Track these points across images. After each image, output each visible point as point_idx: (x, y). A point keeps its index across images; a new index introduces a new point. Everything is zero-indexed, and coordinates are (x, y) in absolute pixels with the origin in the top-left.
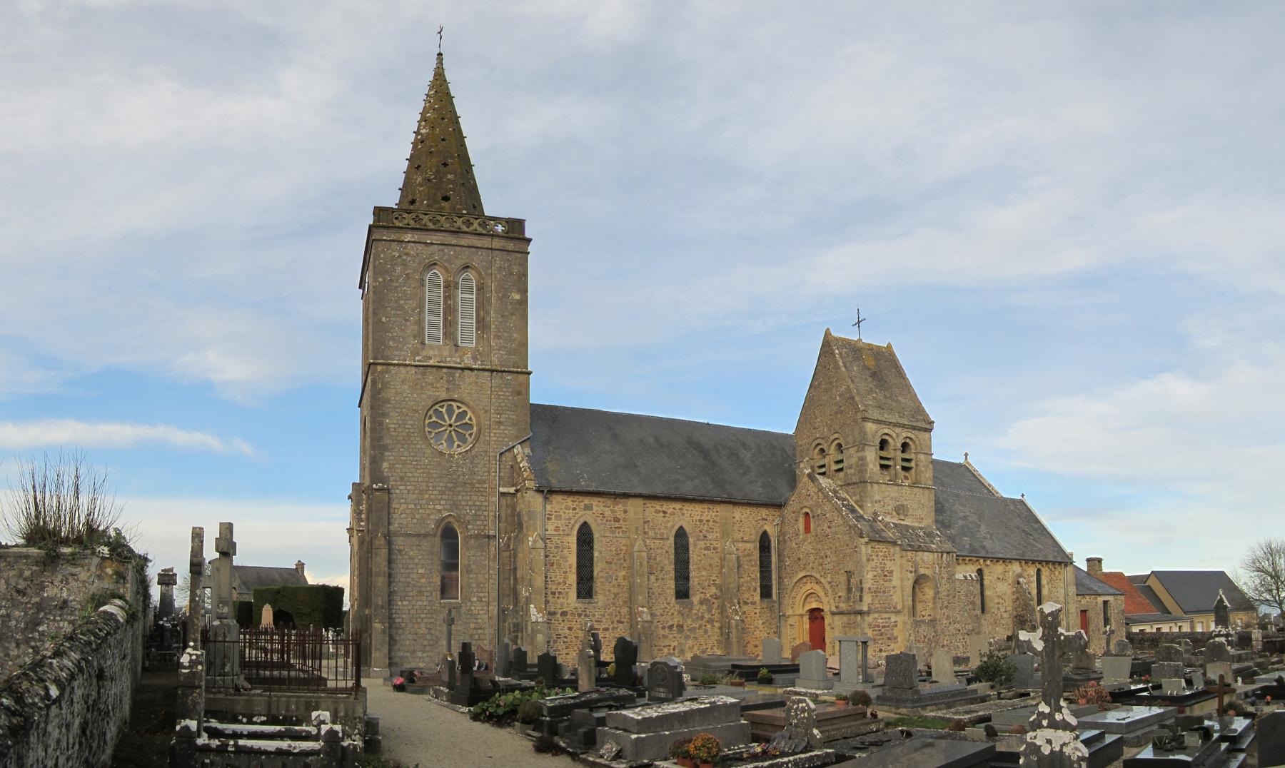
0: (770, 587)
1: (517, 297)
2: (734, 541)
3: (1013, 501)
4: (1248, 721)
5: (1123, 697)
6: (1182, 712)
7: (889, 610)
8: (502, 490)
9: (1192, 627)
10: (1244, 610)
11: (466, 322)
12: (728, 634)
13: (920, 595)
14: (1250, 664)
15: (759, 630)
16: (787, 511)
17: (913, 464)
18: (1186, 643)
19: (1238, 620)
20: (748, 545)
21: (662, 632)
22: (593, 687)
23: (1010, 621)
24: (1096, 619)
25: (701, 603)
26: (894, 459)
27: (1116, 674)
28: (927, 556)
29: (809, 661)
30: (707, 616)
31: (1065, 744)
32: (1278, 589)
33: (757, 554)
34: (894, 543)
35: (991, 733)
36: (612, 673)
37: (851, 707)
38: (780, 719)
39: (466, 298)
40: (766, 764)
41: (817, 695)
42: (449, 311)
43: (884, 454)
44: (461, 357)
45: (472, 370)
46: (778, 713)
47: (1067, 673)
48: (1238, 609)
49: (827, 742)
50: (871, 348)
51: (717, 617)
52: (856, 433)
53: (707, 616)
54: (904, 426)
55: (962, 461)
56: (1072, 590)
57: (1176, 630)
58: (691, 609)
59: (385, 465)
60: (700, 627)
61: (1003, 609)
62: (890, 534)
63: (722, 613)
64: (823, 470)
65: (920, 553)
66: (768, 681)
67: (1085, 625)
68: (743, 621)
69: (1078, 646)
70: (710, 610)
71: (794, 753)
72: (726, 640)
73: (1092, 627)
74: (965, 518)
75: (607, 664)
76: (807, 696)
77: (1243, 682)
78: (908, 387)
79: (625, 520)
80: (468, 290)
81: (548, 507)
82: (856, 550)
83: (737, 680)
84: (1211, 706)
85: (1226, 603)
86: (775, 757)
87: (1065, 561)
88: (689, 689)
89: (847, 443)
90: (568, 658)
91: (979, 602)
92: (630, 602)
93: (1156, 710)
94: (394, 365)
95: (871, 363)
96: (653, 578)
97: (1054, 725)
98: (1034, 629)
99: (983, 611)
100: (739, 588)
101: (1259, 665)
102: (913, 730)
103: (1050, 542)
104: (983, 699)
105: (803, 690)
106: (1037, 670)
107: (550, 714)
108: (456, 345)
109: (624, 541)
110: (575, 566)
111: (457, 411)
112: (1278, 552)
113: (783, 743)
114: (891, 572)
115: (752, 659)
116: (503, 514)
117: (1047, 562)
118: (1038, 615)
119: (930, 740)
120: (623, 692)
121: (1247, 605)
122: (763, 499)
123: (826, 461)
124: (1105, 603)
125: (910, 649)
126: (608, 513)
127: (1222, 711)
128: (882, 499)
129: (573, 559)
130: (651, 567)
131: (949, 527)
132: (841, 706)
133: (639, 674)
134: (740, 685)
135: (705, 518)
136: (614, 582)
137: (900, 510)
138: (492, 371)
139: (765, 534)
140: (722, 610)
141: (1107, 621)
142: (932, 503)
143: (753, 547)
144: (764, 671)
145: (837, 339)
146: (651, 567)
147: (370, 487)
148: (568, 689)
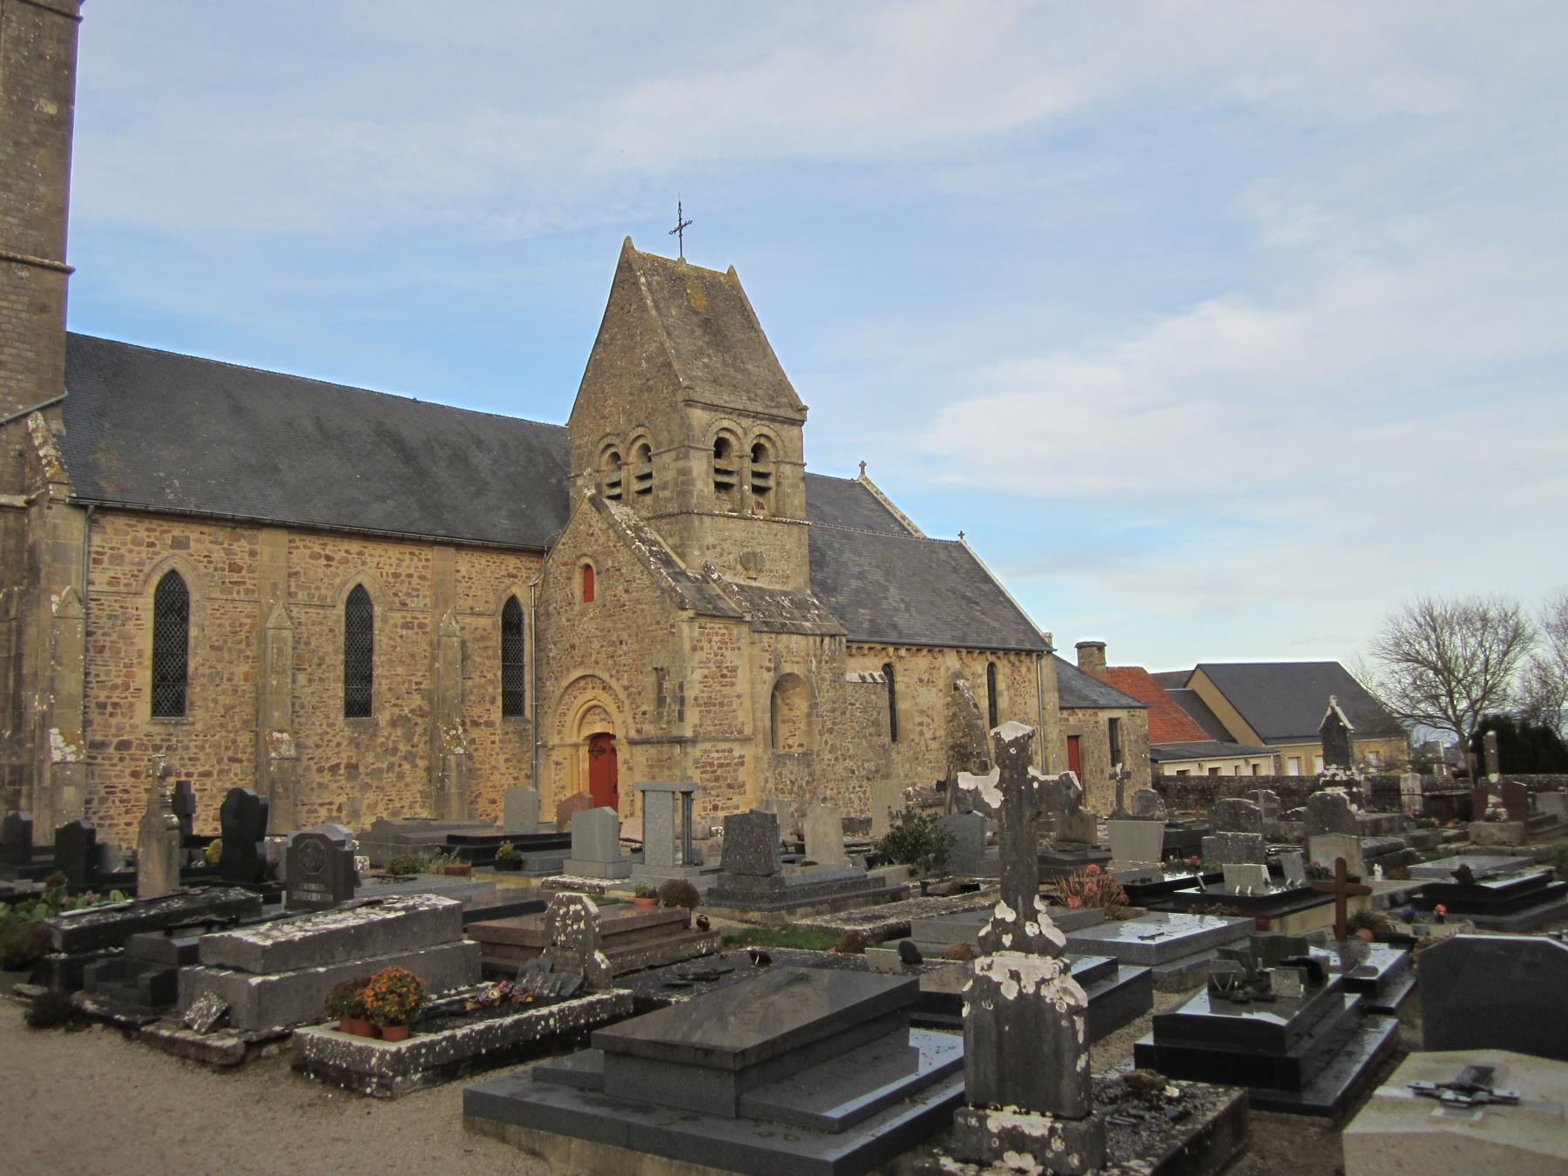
0: (521, 695)
1: (51, 109)
2: (457, 613)
3: (945, 545)
4: (1398, 953)
5: (1150, 896)
6: (1265, 928)
9: (1279, 766)
10: (1381, 734)
12: (442, 780)
13: (784, 710)
14: (1400, 839)
16: (553, 563)
17: (771, 482)
18: (1268, 798)
19: (1371, 755)
20: (482, 621)
21: (318, 778)
22: (176, 887)
23: (942, 756)
24: (1097, 751)
25: (394, 723)
27: (1135, 852)
28: (797, 642)
29: (588, 828)
30: (403, 748)
31: (1043, 981)
32: (1450, 694)
33: (497, 638)
34: (739, 620)
35: (911, 958)
36: (216, 859)
37: (662, 909)
38: (534, 934)
40: (508, 1020)
41: (602, 889)
43: (722, 464)
46: (531, 923)
47: (1044, 849)
48: (1370, 734)
49: (620, 976)
50: (700, 274)
51: (422, 748)
52: (674, 427)
53: (403, 748)
54: (756, 416)
55: (852, 474)
56: (1052, 699)
57: (1247, 772)
58: (375, 735)
60: (390, 768)
61: (929, 735)
62: (731, 604)
64: (617, 491)
65: (784, 637)
66: (515, 866)
67: (1076, 761)
68: (470, 757)
69: (1065, 799)
70: (408, 737)
71: (560, 999)
72: (438, 795)
73: (1088, 767)
74: (861, 576)
75: (206, 841)
76: (586, 891)
77: (1385, 874)
78: (763, 348)
79: (251, 569)
83: (458, 864)
84: (1322, 919)
85: (1345, 721)
86: (525, 1006)
87: (1038, 648)
88: (367, 883)
89: (659, 444)
90: (121, 834)
91: (885, 720)
92: (257, 722)
93: (1213, 923)
95: (700, 302)
96: (302, 678)
97: (1024, 945)
98: (984, 769)
99: (894, 737)
100: (464, 695)
101: (1416, 842)
102: (773, 951)
104: (896, 895)
106: (991, 843)
107: (66, 948)
112: (1448, 622)
113: (540, 980)
114: (734, 670)
115: (484, 826)
117: (1007, 651)
118: (991, 745)
119: (803, 970)
120: (236, 894)
121: (1385, 725)
122: (511, 540)
123: (622, 475)
125: (768, 804)
126: (218, 554)
127: (1345, 930)
128: (720, 543)
129: (146, 642)
130: (300, 657)
131: (833, 591)
132: (645, 908)
133: (269, 858)
134: (463, 873)
135: (403, 570)
136: (226, 685)
137: (750, 562)
139: (512, 603)
140: (432, 736)
141: (1116, 756)
143: (491, 626)
144: (507, 847)
145: (644, 258)
146: (300, 657)
148: (115, 893)
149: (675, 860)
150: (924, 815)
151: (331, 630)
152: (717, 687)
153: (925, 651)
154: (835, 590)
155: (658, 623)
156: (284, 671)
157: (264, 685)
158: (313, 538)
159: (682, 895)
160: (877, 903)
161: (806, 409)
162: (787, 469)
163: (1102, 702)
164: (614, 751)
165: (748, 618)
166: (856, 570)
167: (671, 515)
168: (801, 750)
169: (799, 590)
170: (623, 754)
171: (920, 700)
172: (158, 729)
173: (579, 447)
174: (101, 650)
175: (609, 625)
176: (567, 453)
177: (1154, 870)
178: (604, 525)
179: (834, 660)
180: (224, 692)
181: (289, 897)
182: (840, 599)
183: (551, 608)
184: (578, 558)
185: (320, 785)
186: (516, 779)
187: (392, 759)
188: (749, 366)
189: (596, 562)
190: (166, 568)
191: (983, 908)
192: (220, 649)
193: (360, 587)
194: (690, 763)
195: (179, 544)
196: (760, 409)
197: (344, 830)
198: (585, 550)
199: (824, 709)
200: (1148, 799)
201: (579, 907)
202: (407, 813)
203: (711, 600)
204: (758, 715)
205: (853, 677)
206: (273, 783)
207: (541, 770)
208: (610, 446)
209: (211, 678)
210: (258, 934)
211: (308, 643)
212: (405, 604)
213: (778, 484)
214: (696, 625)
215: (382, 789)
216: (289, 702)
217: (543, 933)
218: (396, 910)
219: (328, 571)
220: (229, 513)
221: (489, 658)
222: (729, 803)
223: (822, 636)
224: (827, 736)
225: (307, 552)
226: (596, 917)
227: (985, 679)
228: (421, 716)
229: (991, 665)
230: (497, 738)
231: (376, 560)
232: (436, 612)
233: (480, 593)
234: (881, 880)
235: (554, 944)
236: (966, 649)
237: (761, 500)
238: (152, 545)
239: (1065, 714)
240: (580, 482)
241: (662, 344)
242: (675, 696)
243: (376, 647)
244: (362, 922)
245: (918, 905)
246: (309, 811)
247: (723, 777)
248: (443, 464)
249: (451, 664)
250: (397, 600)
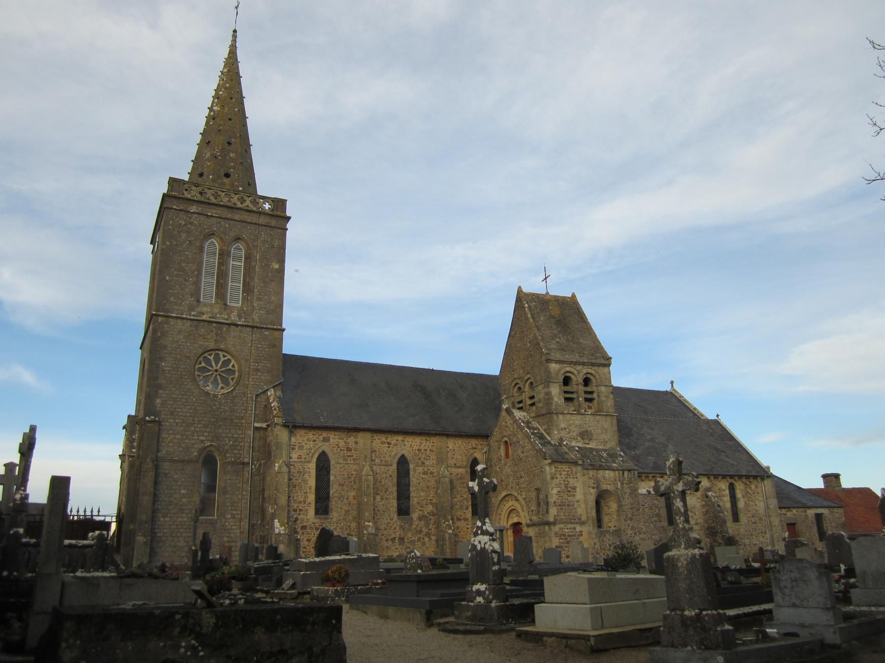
1: (276, 266)
8: (256, 425)
11: (235, 286)
12: (442, 546)
16: (493, 440)
17: (595, 396)
20: (460, 470)
21: (386, 544)
26: (577, 392)
28: (608, 474)
34: (575, 463)
39: (237, 264)
42: (222, 276)
43: (568, 388)
44: (229, 315)
45: (237, 325)
50: (557, 299)
51: (433, 531)
54: (584, 364)
55: (668, 388)
56: (773, 502)
58: (411, 524)
59: (158, 401)
60: (419, 539)
63: (437, 528)
64: (521, 405)
65: (601, 472)
68: (456, 535)
70: (427, 525)
79: (356, 450)
80: (238, 259)
81: (293, 439)
89: (536, 381)
92: (359, 518)
94: (171, 317)
108: (225, 304)
109: (355, 467)
110: (314, 487)
111: (223, 359)
114: (574, 488)
116: (256, 445)
124: (819, 517)
128: (568, 428)
129: (312, 482)
135: (422, 448)
136: (345, 501)
137: (585, 435)
138: (253, 327)
140: (438, 525)
142: (615, 428)
147: (143, 419)
152: (565, 497)
154: (635, 448)
161: (611, 358)
163: (809, 504)
165: (580, 462)
166: (649, 437)
167: (543, 415)
172: (317, 520)
174: (295, 486)
180: (345, 504)
182: (637, 452)
185: (387, 547)
190: (320, 451)
192: (343, 485)
193: (403, 456)
194: (553, 534)
195: (326, 440)
206: (365, 545)
208: (517, 384)
209: (339, 498)
213: (599, 396)
220: (345, 426)
224: (629, 522)
227: (727, 492)
237: (590, 405)
238: (315, 441)
239: (784, 511)
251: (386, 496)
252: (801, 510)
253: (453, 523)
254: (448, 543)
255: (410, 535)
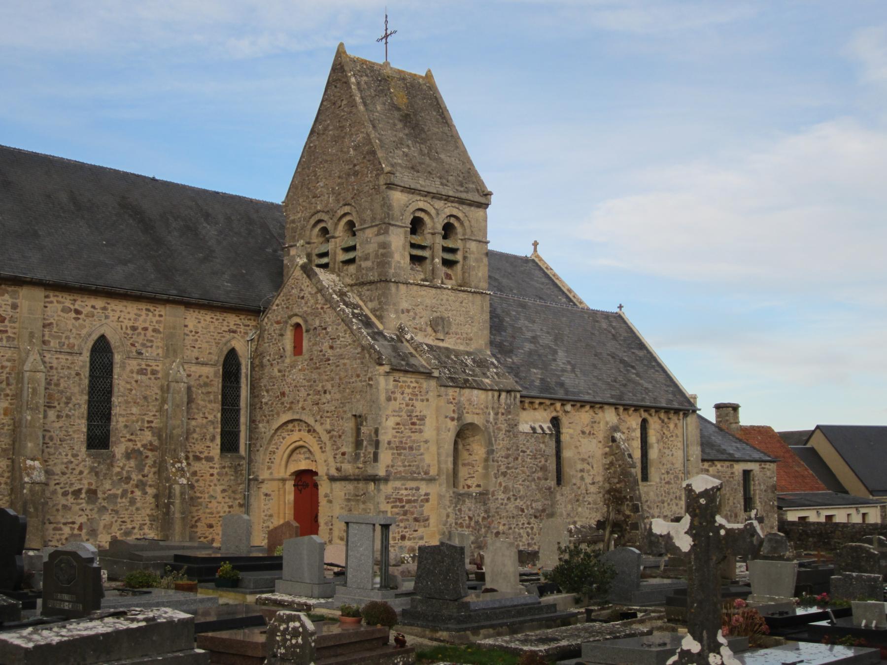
0: (237, 435)
3: (607, 316)
7: (420, 471)
12: (167, 506)
13: (464, 455)
15: (216, 498)
16: (269, 321)
17: (459, 256)
21: (63, 501)
23: (599, 498)
25: (128, 456)
26: (431, 248)
29: (296, 552)
30: (135, 477)
33: (217, 385)
34: (428, 375)
43: (417, 239)
46: (258, 637)
50: (402, 77)
51: (151, 479)
52: (377, 206)
53: (135, 477)
54: (447, 199)
56: (696, 451)
57: (857, 519)
58: (111, 465)
60: (124, 493)
61: (588, 480)
62: (421, 361)
63: (159, 473)
64: (325, 260)
65: (467, 392)
66: (232, 583)
68: (192, 487)
70: (140, 468)
72: (163, 515)
74: (534, 340)
76: (301, 609)
78: (452, 139)
79: (12, 320)
82: (370, 383)
83: (185, 581)
87: (685, 407)
89: (363, 221)
91: (552, 465)
95: (401, 100)
96: (52, 414)
99: (559, 481)
100: (188, 433)
103: (661, 377)
104: (566, 620)
105: (286, 598)
114: (422, 419)
117: (658, 409)
123: (330, 247)
124: (747, 474)
128: (415, 308)
130: (50, 397)
133: (26, 568)
134: (191, 589)
135: (140, 324)
137: (438, 324)
139: (232, 353)
140: (161, 468)
142: (487, 316)
143: (212, 373)
145: (354, 61)
146: (50, 397)
149: (373, 584)
150: (589, 550)
151: (78, 374)
152: (407, 433)
153: (587, 407)
154: (511, 351)
155: (358, 376)
156: (37, 408)
157: (20, 420)
158: (65, 295)
159: (380, 615)
160: (549, 627)
161: (490, 194)
162: (473, 246)
163: (738, 455)
164: (316, 486)
165: (436, 373)
166: (529, 335)
167: (371, 283)
168: (478, 490)
169: (480, 351)
170: (324, 488)
171: (582, 450)
173: (293, 222)
175: (315, 376)
176: (283, 227)
177: (789, 604)
178: (311, 289)
179: (509, 413)
181: (44, 605)
182: (516, 360)
183: (265, 361)
184: (290, 317)
185: (65, 507)
186: (230, 507)
187: (125, 486)
188: (442, 156)
189: (306, 321)
191: (643, 634)
193: (103, 337)
194: (382, 499)
196: (451, 193)
197: (89, 548)
198: (296, 310)
199: (499, 454)
200: (777, 541)
201: (297, 624)
202: (137, 534)
203: (405, 357)
204: (443, 458)
205: (525, 427)
207: (252, 500)
210: (21, 637)
211: (57, 385)
212: (140, 353)
213: (465, 258)
214: (392, 379)
215: (117, 512)
216: (40, 434)
217: (263, 645)
218: (138, 621)
219: (77, 323)
221: (210, 402)
222: (415, 534)
223: (500, 391)
224: (501, 479)
225: (60, 306)
226: (312, 634)
227: (638, 433)
228: (151, 450)
229: (644, 422)
230: (215, 471)
231: (117, 314)
232: (167, 361)
233: (205, 345)
234: (553, 607)
235: (275, 656)
236: (623, 406)
237: (449, 272)
239: (706, 465)
240: (293, 252)
241: (368, 135)
242: (371, 440)
243: (115, 389)
244: (109, 630)
245: (586, 630)
246: (55, 529)
247: (411, 510)
248: (176, 234)
249: (178, 406)
250: (134, 349)
251: (66, 411)
252: (727, 464)
253: (188, 464)
254: (178, 501)
255: (107, 485)
